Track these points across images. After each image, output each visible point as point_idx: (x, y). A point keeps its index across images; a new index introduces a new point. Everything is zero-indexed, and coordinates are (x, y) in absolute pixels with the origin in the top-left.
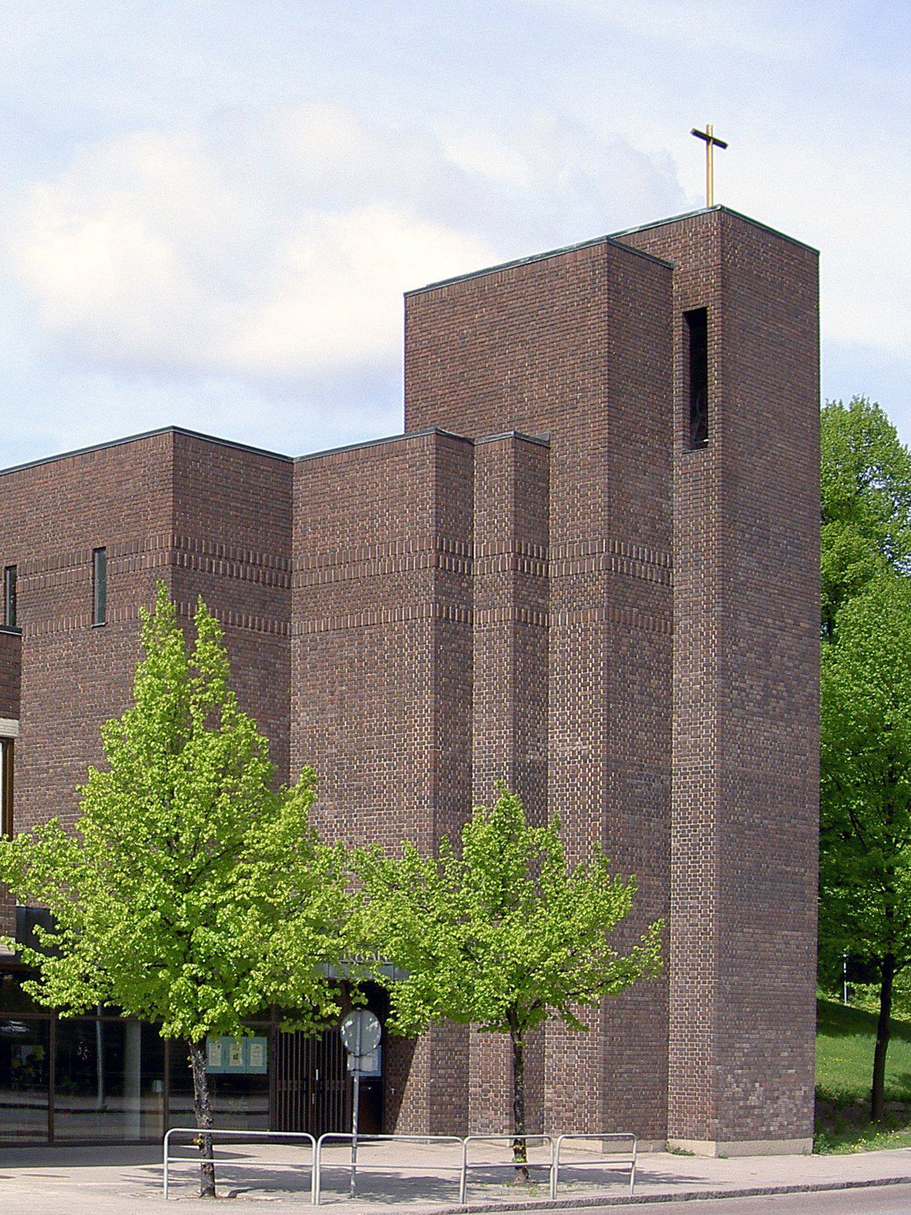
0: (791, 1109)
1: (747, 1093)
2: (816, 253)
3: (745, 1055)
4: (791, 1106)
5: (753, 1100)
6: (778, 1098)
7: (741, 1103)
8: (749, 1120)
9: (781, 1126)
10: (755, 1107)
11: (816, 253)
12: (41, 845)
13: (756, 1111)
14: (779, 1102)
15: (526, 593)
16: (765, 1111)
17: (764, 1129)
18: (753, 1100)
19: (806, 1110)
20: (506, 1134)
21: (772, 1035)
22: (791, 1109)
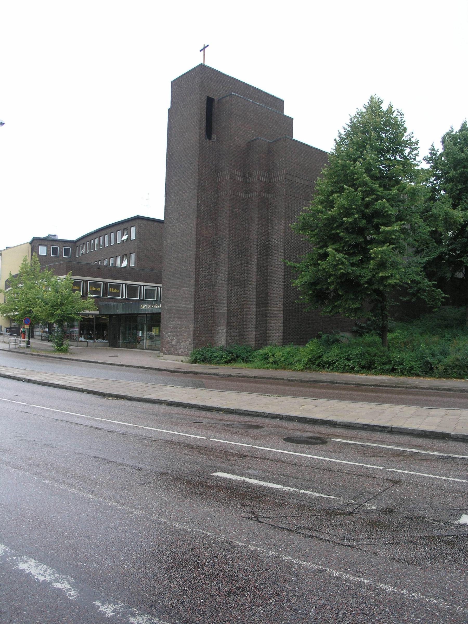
0: (185, 347)
1: (172, 340)
2: (292, 119)
3: (172, 329)
4: (185, 346)
5: (174, 343)
6: (181, 343)
7: (170, 343)
8: (172, 349)
9: (182, 352)
10: (174, 345)
11: (292, 119)
12: (181, 106)
13: (175, 346)
14: (182, 344)
15: (176, 178)
16: (177, 347)
17: (177, 352)
18: (174, 343)
19: (190, 347)
20: (143, 343)
21: (179, 322)
22: (185, 347)
